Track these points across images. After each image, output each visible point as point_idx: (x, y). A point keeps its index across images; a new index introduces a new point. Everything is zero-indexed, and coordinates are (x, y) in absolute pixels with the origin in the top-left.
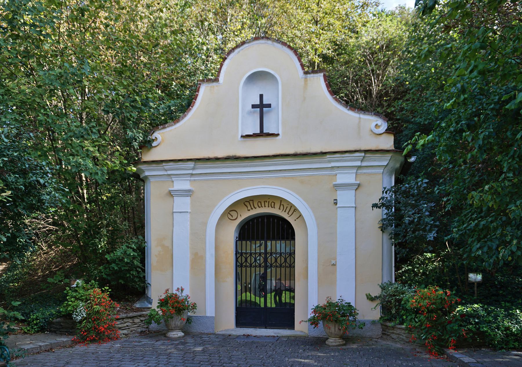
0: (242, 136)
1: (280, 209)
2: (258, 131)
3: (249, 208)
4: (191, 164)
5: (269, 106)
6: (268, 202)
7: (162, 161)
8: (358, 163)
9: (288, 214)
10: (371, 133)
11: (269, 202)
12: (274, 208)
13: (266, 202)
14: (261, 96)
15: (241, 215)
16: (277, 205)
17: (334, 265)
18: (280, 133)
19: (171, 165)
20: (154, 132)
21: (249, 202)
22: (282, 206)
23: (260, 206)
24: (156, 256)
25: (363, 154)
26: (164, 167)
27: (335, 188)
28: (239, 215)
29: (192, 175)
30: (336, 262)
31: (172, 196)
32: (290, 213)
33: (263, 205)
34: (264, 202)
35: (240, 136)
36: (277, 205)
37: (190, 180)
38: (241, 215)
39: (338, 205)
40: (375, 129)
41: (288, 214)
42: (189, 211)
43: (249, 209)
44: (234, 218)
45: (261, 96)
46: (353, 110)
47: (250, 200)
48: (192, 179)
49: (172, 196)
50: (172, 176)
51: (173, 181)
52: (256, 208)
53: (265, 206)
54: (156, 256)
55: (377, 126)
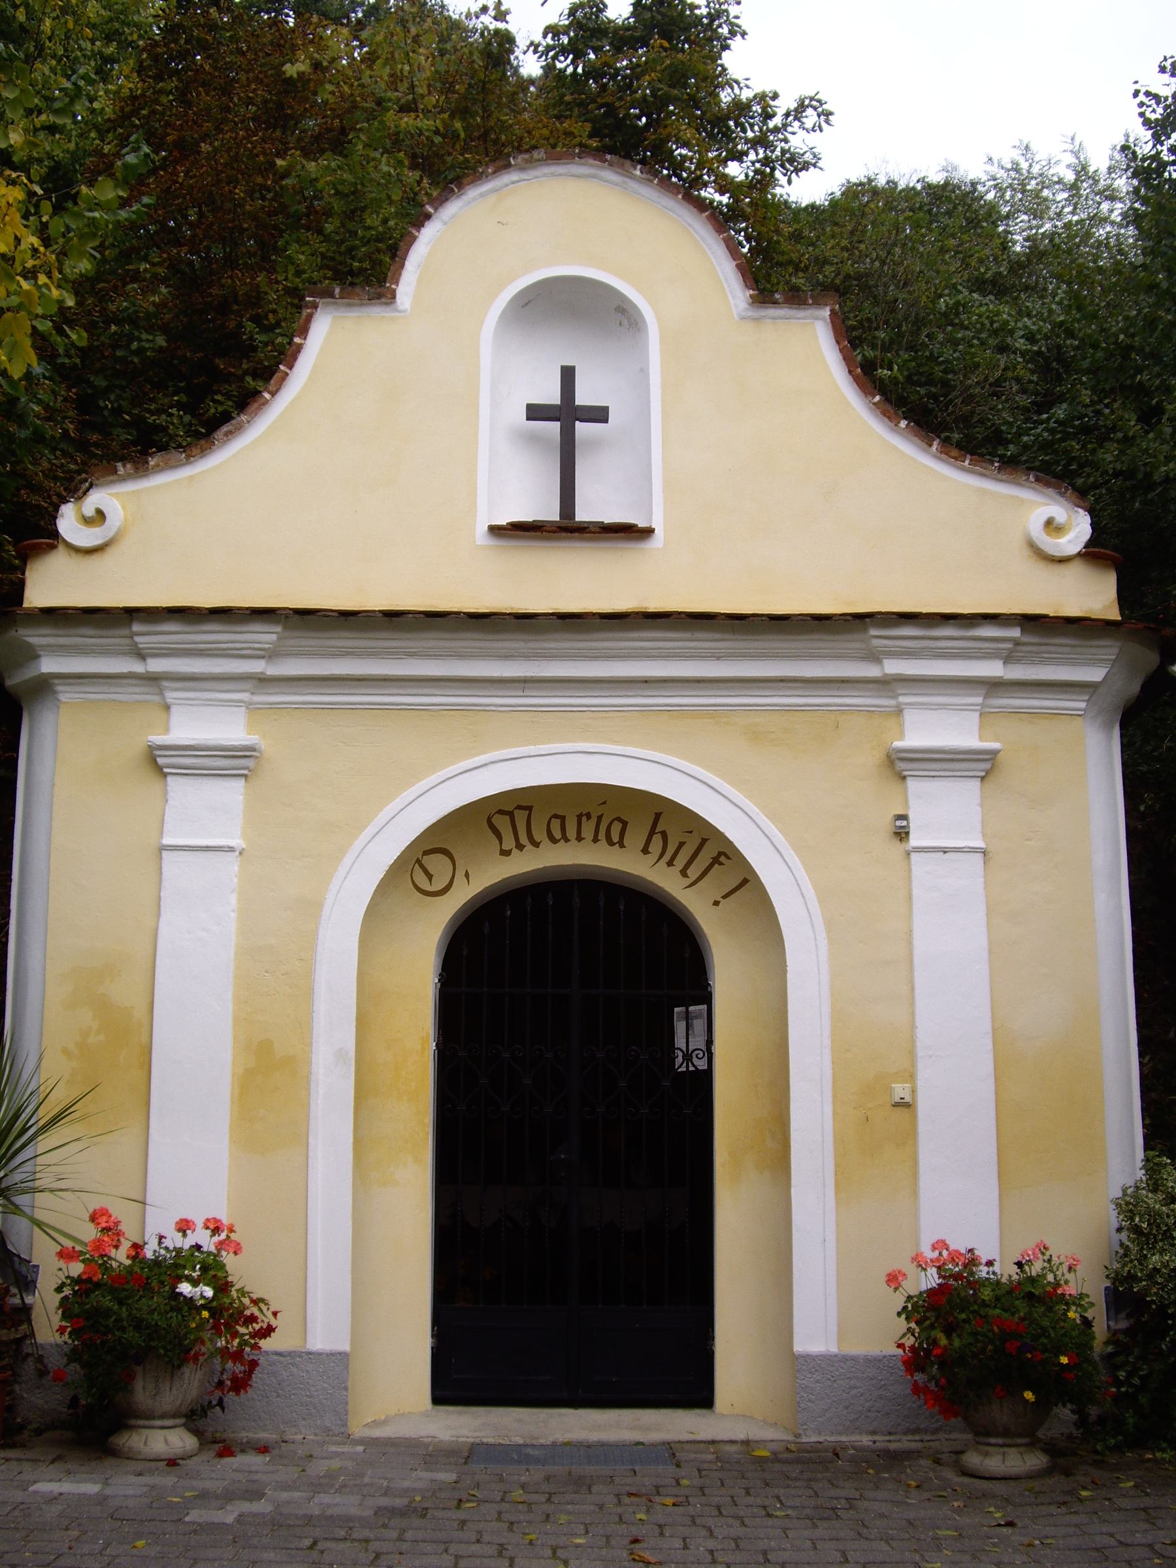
0: (496, 531)
1: (645, 851)
2: (551, 513)
3: (509, 843)
4: (266, 635)
5: (599, 415)
6: (594, 820)
7: (132, 614)
8: (993, 669)
9: (684, 873)
10: (1026, 552)
11: (600, 818)
12: (622, 846)
13: (589, 816)
14: (568, 375)
15: (467, 875)
16: (635, 838)
17: (905, 1105)
18: (657, 524)
19: (173, 633)
20: (91, 486)
21: (511, 814)
22: (657, 840)
23: (557, 834)
24: (66, 1052)
25: (1015, 633)
26: (137, 639)
27: (901, 765)
28: (460, 874)
29: (263, 681)
30: (914, 1091)
31: (161, 772)
32: (693, 872)
33: (571, 832)
34: (579, 817)
35: (482, 528)
36: (635, 838)
37: (249, 705)
38: (467, 875)
39: (914, 841)
40: (1045, 537)
41: (684, 873)
42: (237, 842)
43: (506, 847)
44: (437, 886)
45: (568, 375)
46: (956, 458)
47: (519, 807)
48: (257, 698)
49: (161, 772)
50: (165, 684)
51: (167, 708)
52: (536, 844)
53: (579, 838)
54: (66, 1052)
55: (1050, 525)
